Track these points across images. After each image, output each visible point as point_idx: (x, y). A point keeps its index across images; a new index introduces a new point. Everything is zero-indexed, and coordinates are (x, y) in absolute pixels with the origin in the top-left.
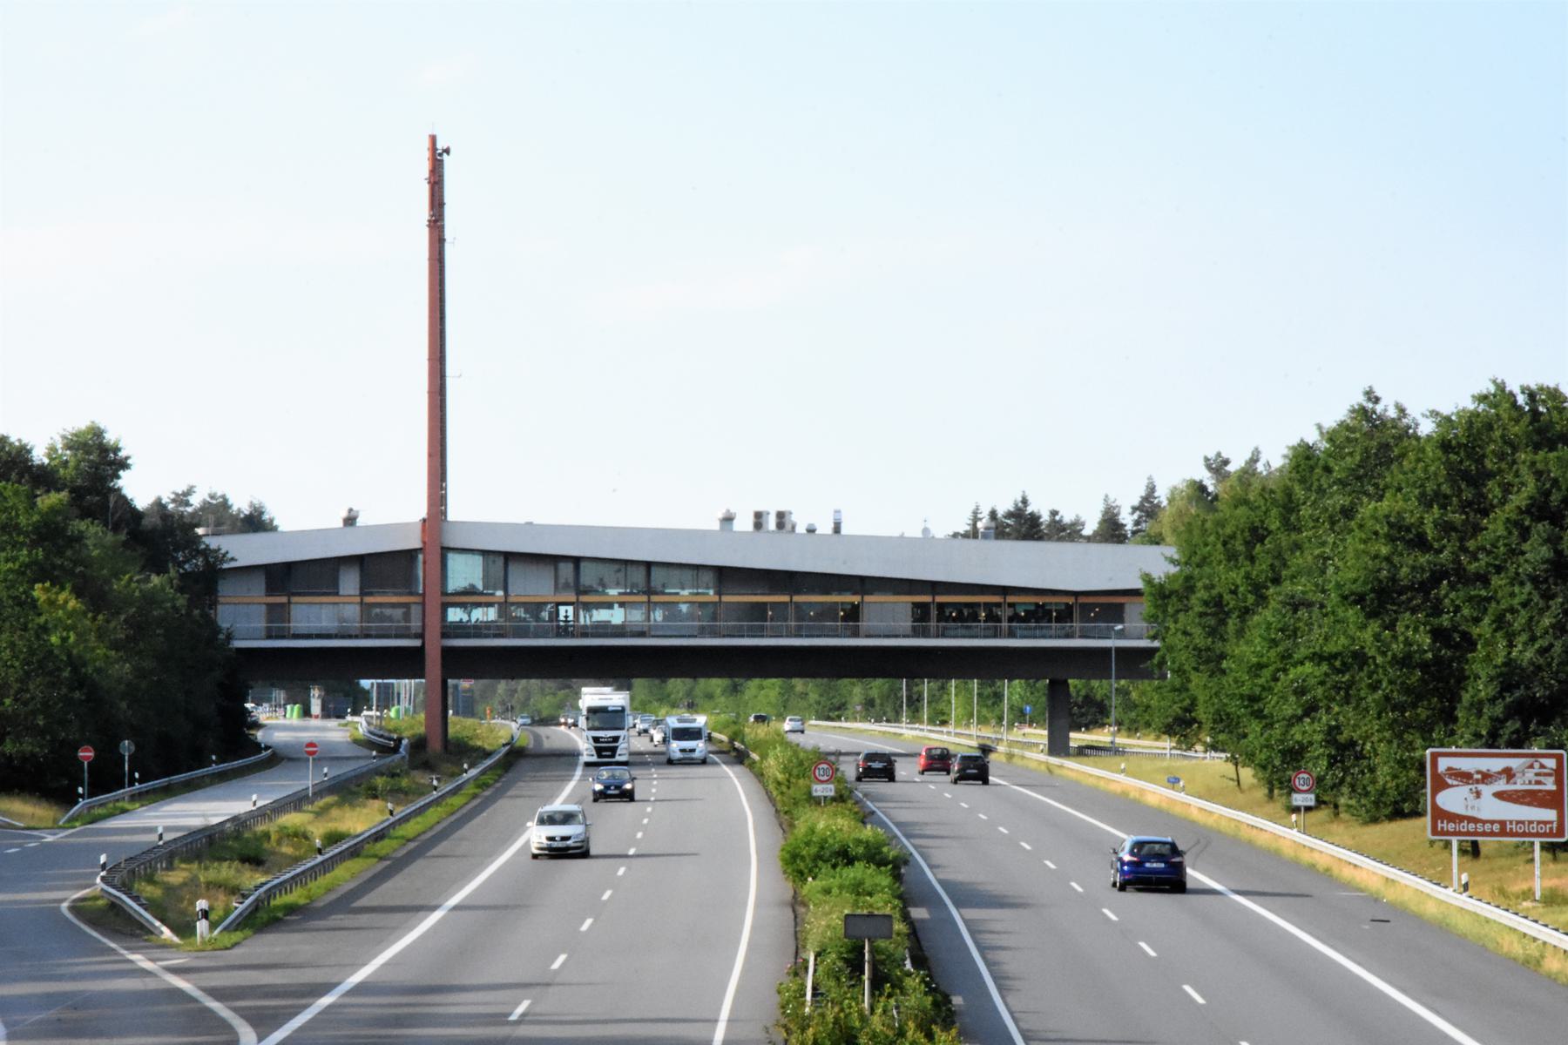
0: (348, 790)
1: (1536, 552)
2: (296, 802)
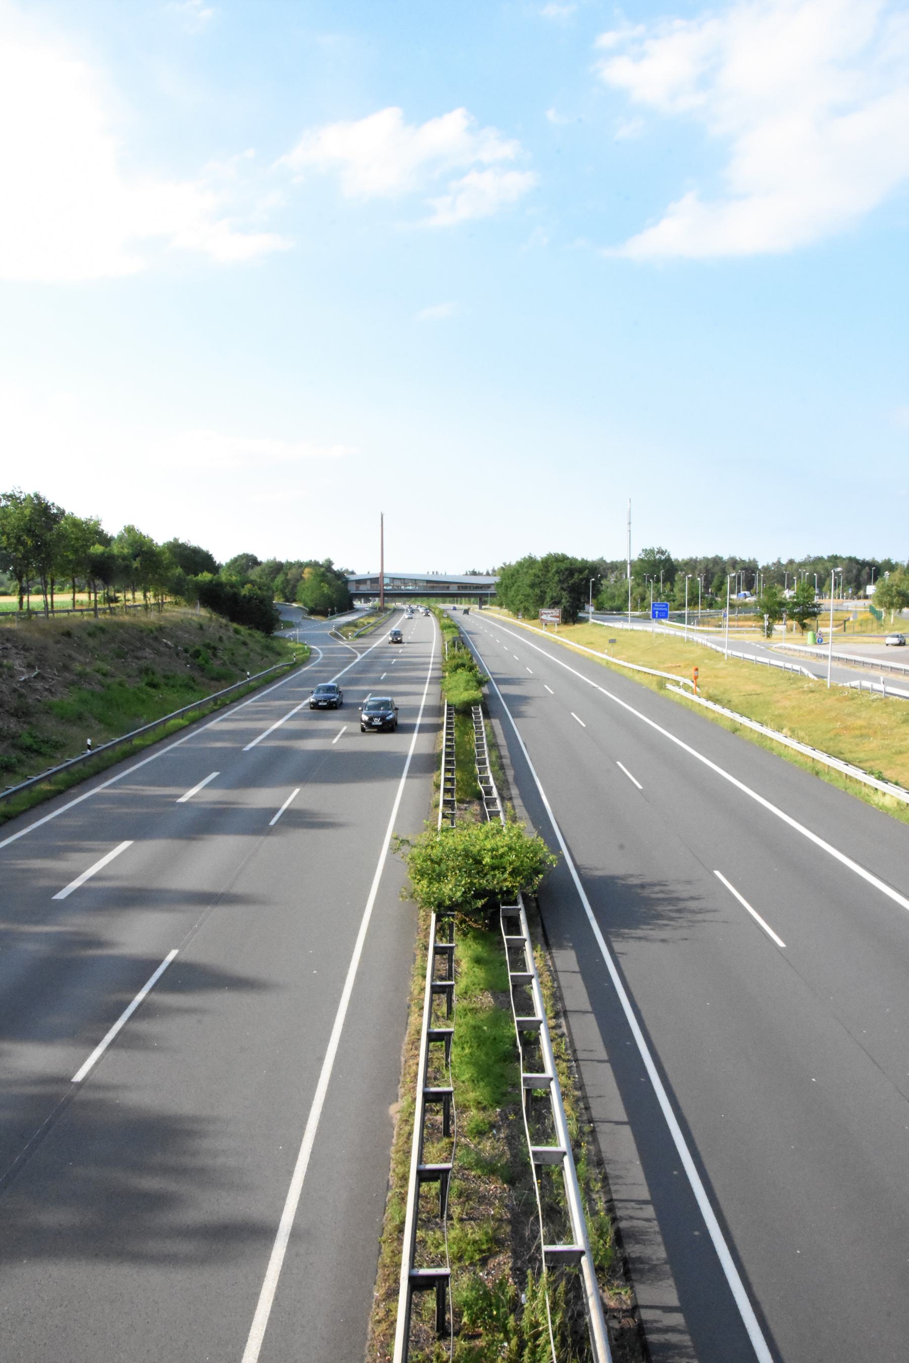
0: (370, 615)
1: (556, 578)
2: (362, 617)
